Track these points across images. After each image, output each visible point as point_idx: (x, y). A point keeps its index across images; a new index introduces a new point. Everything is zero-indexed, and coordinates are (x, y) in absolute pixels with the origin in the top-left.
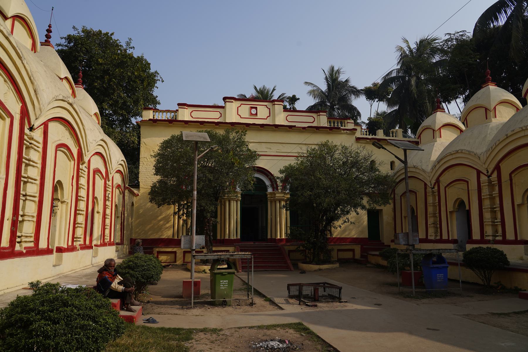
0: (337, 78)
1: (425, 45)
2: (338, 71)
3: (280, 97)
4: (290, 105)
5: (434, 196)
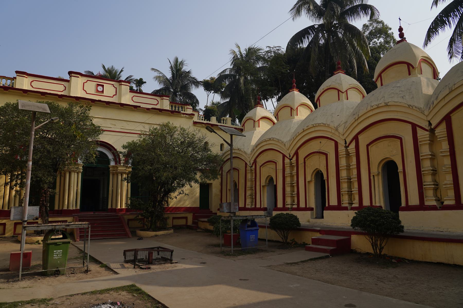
1: (252, 52)
2: (182, 63)
3: (127, 78)
4: (137, 86)
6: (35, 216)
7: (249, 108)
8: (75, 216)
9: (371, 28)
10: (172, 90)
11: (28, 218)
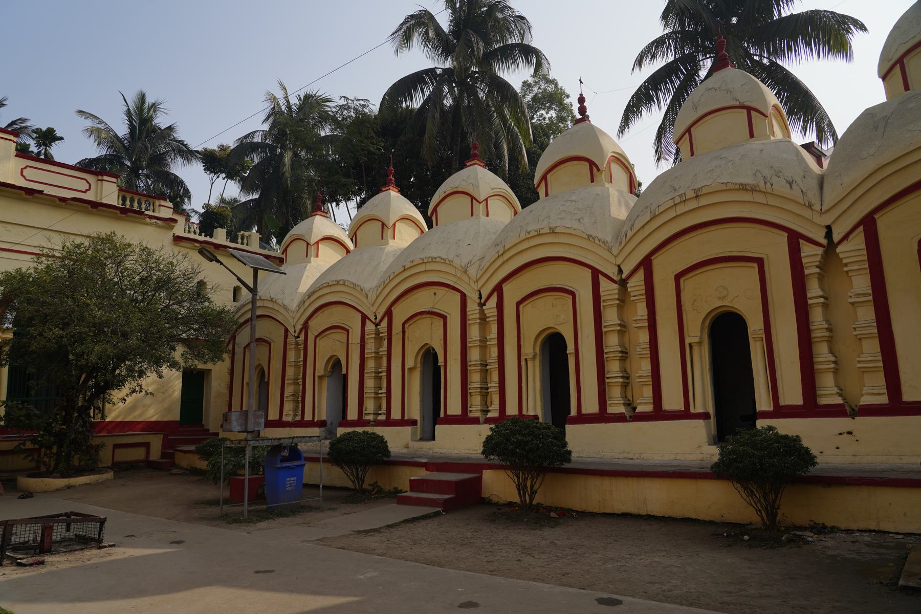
0: (151, 119)
1: (310, 103)
3: (13, 123)
4: (39, 145)
7: (299, 215)
9: (535, 89)
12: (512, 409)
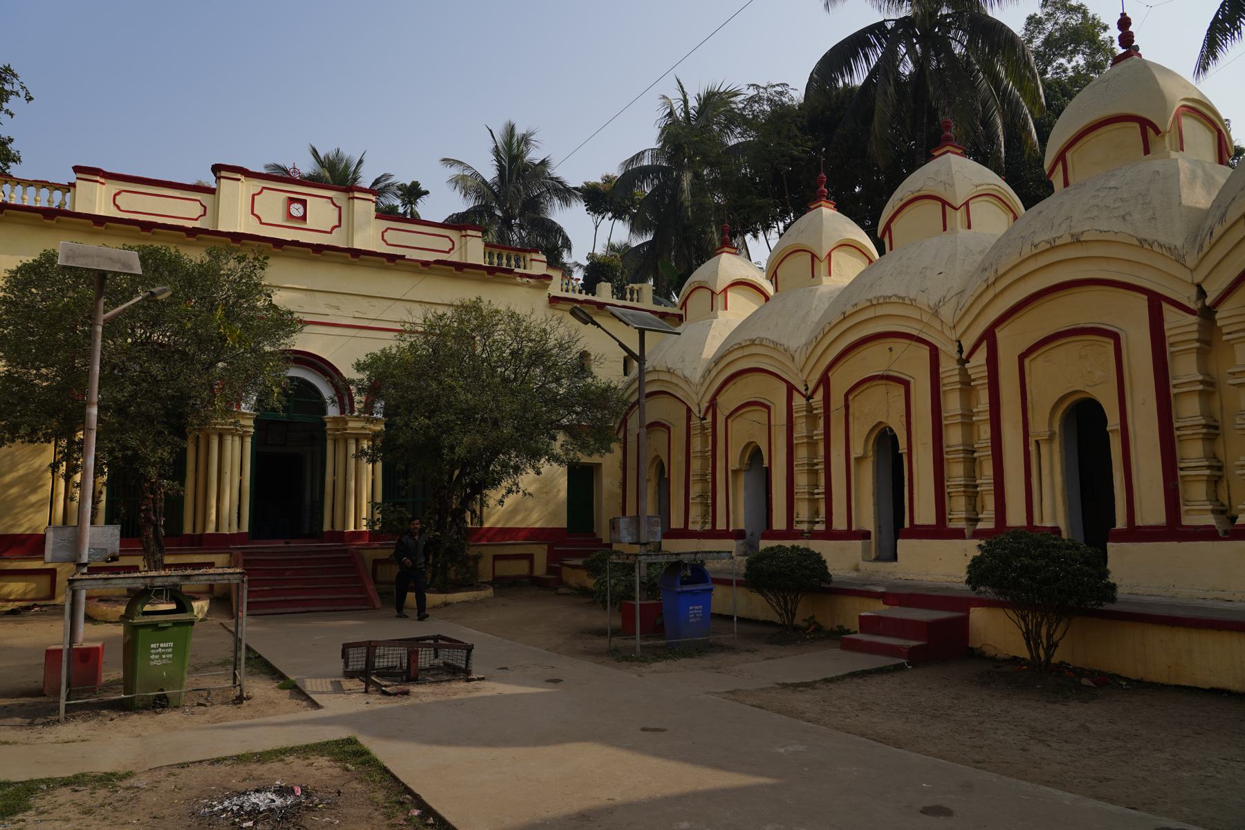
1: (714, 102)
2: (525, 139)
3: (377, 182)
4: (404, 204)
5: (704, 435)
6: (109, 552)
7: (706, 253)
8: (235, 552)
9: (1049, 26)
10: (498, 213)
11: (90, 555)
12: (1016, 517)
